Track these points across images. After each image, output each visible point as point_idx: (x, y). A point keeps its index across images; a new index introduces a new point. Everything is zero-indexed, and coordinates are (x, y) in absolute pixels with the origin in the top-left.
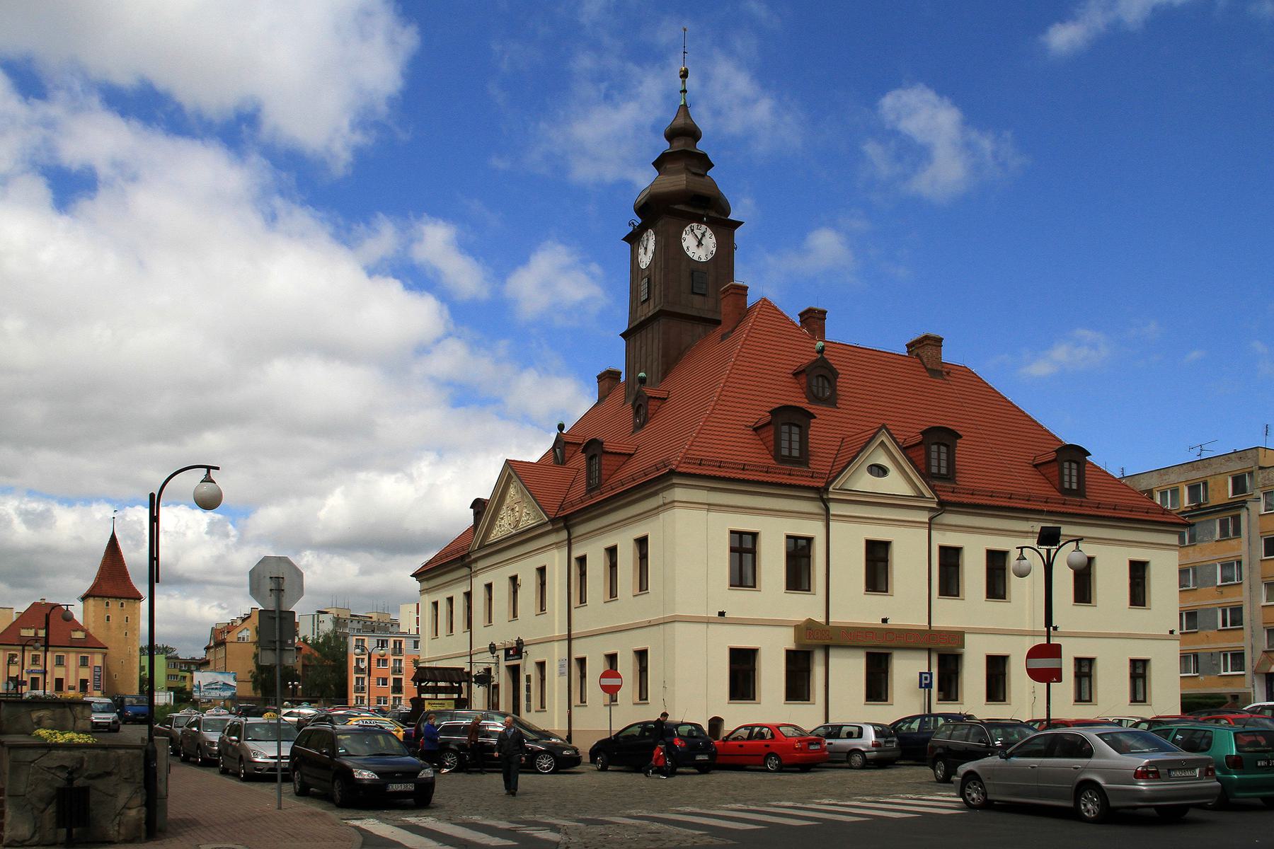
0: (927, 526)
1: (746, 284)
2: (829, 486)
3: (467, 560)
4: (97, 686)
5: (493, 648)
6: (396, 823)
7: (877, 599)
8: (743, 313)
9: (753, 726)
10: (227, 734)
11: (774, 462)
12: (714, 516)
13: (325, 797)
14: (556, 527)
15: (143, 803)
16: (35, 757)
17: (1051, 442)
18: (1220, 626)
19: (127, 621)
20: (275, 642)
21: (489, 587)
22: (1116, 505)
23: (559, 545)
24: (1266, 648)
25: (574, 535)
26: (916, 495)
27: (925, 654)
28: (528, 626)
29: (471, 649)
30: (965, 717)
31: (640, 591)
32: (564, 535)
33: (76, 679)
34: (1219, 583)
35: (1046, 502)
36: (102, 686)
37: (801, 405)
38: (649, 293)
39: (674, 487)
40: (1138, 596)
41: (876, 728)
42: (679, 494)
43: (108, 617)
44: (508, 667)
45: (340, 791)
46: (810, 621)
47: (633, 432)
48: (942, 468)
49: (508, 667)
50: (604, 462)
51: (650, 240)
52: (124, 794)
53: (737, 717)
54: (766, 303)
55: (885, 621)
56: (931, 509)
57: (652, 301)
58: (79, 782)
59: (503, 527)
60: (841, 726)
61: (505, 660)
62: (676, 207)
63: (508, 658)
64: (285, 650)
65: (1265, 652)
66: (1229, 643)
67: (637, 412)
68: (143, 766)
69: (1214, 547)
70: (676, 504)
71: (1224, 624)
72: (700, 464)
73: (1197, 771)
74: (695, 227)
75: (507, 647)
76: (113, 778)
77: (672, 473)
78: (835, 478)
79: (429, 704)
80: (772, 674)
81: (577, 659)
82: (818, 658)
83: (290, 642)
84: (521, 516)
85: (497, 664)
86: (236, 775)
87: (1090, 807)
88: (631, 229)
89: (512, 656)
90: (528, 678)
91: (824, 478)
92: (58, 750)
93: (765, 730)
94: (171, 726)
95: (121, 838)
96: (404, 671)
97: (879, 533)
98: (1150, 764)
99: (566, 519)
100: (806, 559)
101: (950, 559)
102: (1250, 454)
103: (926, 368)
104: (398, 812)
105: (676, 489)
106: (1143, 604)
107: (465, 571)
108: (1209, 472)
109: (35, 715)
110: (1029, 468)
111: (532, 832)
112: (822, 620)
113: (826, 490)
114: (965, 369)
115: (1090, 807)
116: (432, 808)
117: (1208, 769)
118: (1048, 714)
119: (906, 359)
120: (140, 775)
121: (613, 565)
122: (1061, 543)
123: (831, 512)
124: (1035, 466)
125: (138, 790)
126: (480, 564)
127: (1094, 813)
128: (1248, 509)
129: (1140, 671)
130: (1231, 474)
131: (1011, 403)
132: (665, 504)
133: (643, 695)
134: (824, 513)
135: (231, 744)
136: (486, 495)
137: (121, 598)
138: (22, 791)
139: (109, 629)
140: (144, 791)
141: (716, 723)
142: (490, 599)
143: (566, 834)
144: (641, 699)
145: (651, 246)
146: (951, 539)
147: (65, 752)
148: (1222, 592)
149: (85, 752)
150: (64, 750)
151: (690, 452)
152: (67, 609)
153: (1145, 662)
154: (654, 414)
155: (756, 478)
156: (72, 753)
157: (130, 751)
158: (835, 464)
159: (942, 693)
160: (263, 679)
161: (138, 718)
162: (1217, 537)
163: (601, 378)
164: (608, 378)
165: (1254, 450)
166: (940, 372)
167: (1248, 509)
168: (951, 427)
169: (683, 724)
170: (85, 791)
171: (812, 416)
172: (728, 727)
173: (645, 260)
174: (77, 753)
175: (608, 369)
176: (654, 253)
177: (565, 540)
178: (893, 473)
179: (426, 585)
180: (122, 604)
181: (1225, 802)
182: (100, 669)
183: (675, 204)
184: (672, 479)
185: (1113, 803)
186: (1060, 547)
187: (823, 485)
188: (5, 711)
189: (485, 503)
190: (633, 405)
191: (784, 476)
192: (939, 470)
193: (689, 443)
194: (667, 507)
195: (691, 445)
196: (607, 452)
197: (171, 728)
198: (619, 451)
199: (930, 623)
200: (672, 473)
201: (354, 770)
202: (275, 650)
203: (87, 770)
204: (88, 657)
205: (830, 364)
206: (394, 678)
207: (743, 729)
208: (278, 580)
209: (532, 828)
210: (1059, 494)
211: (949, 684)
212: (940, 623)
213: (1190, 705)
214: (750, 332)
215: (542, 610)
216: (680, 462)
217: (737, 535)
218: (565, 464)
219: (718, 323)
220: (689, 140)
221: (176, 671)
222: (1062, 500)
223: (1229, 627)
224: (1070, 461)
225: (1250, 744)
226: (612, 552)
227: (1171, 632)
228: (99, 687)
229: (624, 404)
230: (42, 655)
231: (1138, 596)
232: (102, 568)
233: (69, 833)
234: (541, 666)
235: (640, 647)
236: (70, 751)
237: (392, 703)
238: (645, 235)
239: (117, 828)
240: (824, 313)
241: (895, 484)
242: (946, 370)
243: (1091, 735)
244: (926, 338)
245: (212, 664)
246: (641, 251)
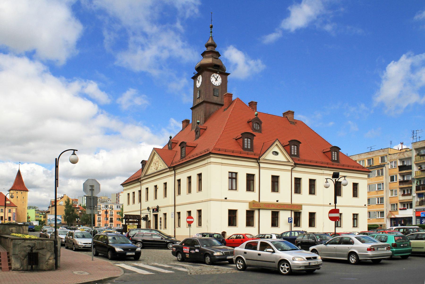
0: (291, 171)
2: (260, 158)
3: (140, 180)
4: (14, 219)
5: (148, 209)
6: (131, 265)
7: (275, 194)
8: (231, 102)
9: (237, 235)
10: (68, 236)
11: (242, 150)
12: (223, 167)
13: (105, 257)
14: (171, 170)
15: (54, 258)
16: (21, 242)
17: (329, 145)
18: (377, 203)
19: (23, 198)
20: (91, 207)
21: (147, 189)
22: (349, 166)
23: (171, 176)
24: (390, 210)
25: (176, 173)
26: (287, 161)
27: (290, 212)
28: (161, 202)
29: (141, 209)
30: (304, 232)
31: (199, 191)
32: (173, 172)
33: (7, 217)
34: (377, 190)
35: (327, 164)
36: (15, 219)
37: (250, 132)
39: (211, 158)
40: (355, 194)
41: (277, 235)
42: (212, 160)
43: (17, 197)
44: (154, 215)
45: (110, 255)
46: (254, 201)
47: (195, 140)
48: (293, 152)
49: (154, 215)
50: (186, 149)
51: (200, 78)
52: (48, 255)
53: (231, 232)
54: (238, 99)
55: (277, 201)
56: (292, 166)
57: (201, 98)
58: (34, 251)
59: (152, 170)
60: (265, 235)
61: (153, 212)
62: (209, 68)
63: (154, 212)
64: (94, 209)
65: (390, 211)
66: (380, 209)
67: (196, 132)
68: (54, 246)
69: (375, 179)
70: (211, 163)
71: (378, 203)
72: (219, 150)
73: (385, 248)
74: (215, 75)
75: (153, 208)
76: (45, 250)
77: (210, 153)
78: (262, 155)
79: (129, 226)
80: (241, 218)
81: (177, 213)
82: (256, 213)
83: (96, 206)
84: (158, 166)
85: (150, 214)
86: (72, 249)
87: (353, 260)
88: (194, 75)
89: (155, 211)
90: (161, 218)
91: (258, 155)
92: (27, 241)
93: (241, 236)
94: (46, 232)
95: (48, 269)
96: (113, 215)
97: (276, 173)
98: (372, 246)
99: (174, 167)
100: (277, 183)
101: (298, 181)
102: (386, 150)
103: (289, 121)
104: (130, 262)
106: (314, 194)
107: (139, 184)
108: (374, 155)
109: (11, 229)
110: (322, 153)
111: (177, 268)
112: (257, 200)
113: (259, 159)
114: (301, 122)
115: (353, 260)
116: (140, 260)
117: (388, 248)
118: (335, 231)
119: (282, 118)
120: (53, 249)
121: (190, 183)
122: (339, 178)
123: (261, 166)
124: (324, 153)
125: (53, 254)
126: (144, 181)
127: (354, 261)
128: (385, 167)
129: (355, 217)
130: (380, 156)
131: (315, 133)
132: (208, 163)
133: (200, 224)
134: (258, 166)
135: (70, 239)
136: (146, 159)
137: (21, 191)
138: (17, 253)
139: (17, 200)
140: (54, 254)
141: (224, 233)
142: (147, 193)
143: (188, 269)
144: (199, 225)
145: (201, 81)
146: (298, 176)
147: (30, 241)
148: (377, 193)
149: (36, 241)
150: (29, 241)
151: (216, 146)
152: (12, 194)
153: (314, 214)
155: (237, 155)
156: (32, 241)
157: (49, 241)
158: (262, 151)
159: (295, 224)
160: (67, 217)
161: (30, 230)
162: (376, 175)
164: (186, 122)
165: (387, 149)
166: (295, 122)
167: (385, 167)
168: (298, 140)
169: (215, 234)
170: (37, 254)
171: (254, 136)
172: (228, 235)
173: (198, 85)
174: (33, 242)
175: (185, 119)
176: (202, 83)
179: (125, 188)
180: (22, 193)
181: (392, 258)
182: (15, 214)
183: (208, 67)
184: (210, 155)
185: (360, 258)
186: (339, 179)
187: (258, 157)
188: (2, 227)
189: (145, 162)
190: (195, 131)
191: (238, 154)
192: (294, 153)
193: (215, 143)
194: (208, 164)
195: (216, 144)
196: (188, 146)
197: (46, 233)
198: (193, 146)
199: (291, 202)
201: (115, 248)
202: (91, 209)
203: (37, 247)
204: (11, 209)
205: (260, 119)
206: (110, 218)
207: (234, 236)
208: (92, 186)
209: (176, 267)
210: (331, 162)
211: (297, 221)
212: (295, 202)
213: (371, 228)
214: (234, 108)
215: (165, 197)
216: (213, 150)
217: (273, 177)
218: (172, 149)
219: (222, 105)
220: (213, 47)
221: (38, 215)
222: (332, 163)
223: (379, 204)
224: (335, 151)
225: (398, 240)
227: (365, 205)
228: (15, 219)
229: (191, 130)
230: (4, 209)
231: (355, 194)
233: (32, 267)
234: (165, 214)
235: (199, 209)
236: (31, 241)
237: (109, 226)
238: (198, 77)
239: (46, 266)
240: (256, 103)
241: (282, 157)
242: (295, 122)
243: (353, 237)
244: (289, 111)
245: (51, 212)
246: (197, 82)
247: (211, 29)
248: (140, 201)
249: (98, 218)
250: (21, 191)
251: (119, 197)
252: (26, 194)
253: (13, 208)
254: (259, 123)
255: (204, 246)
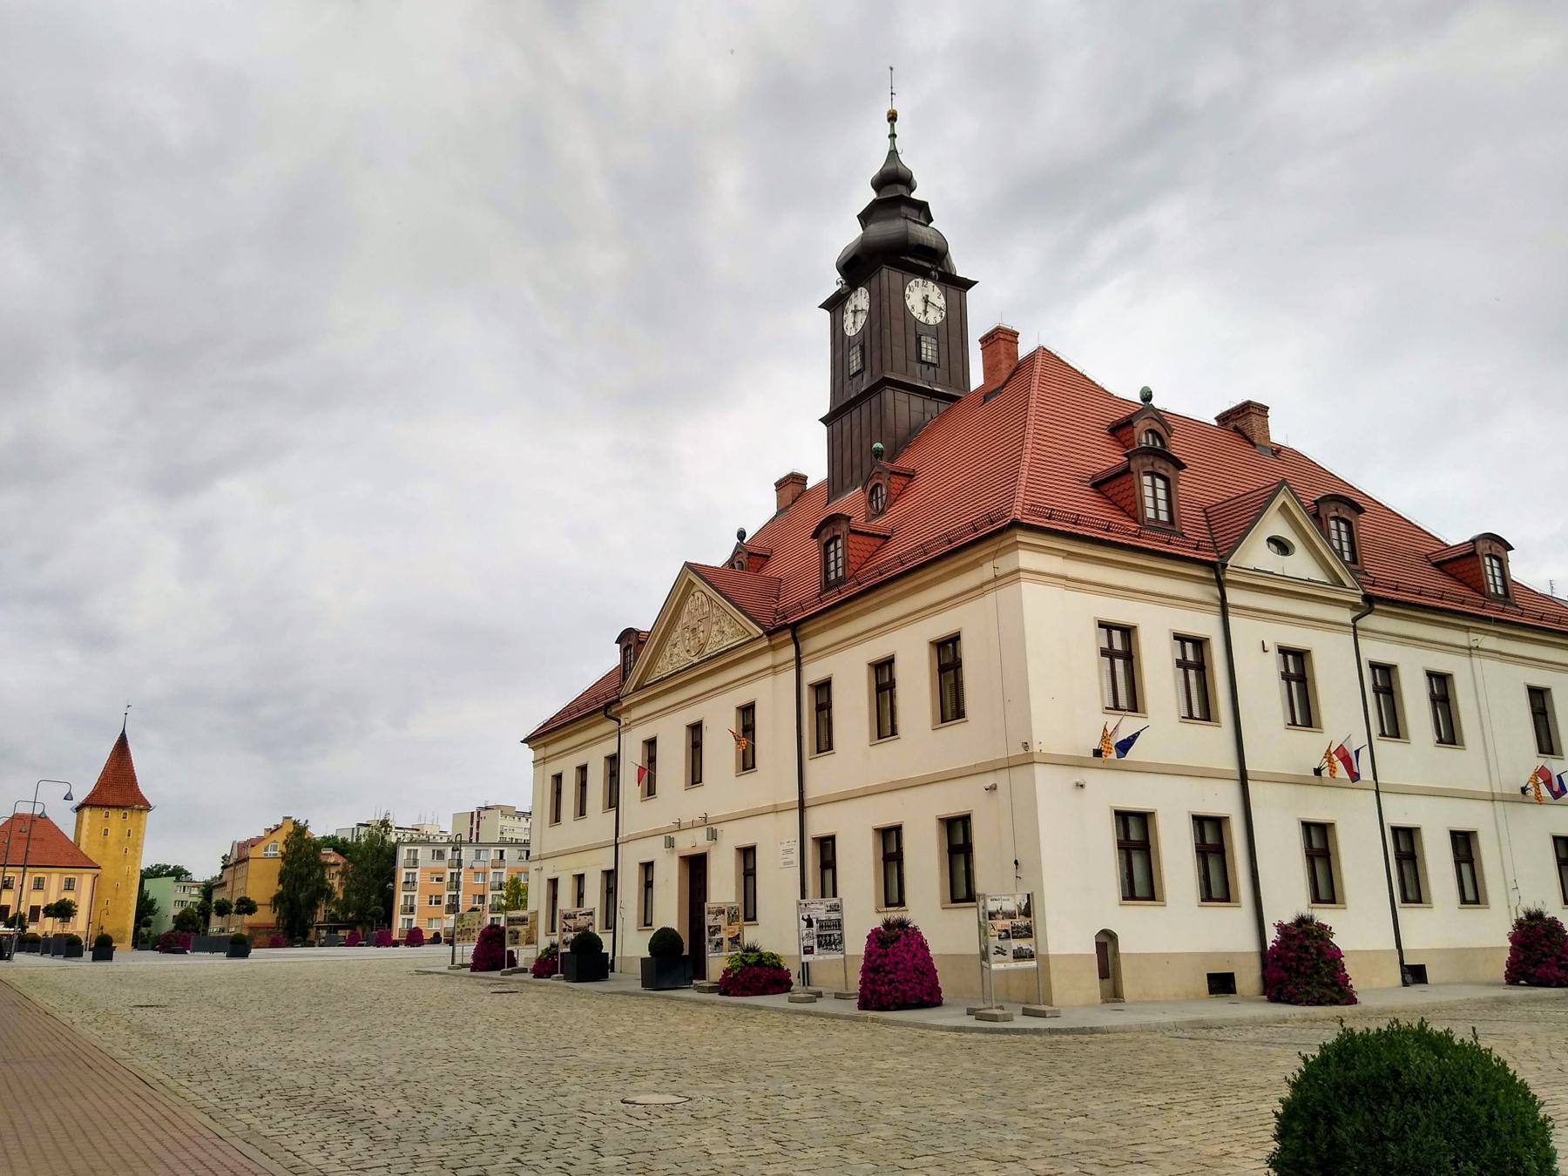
1: (1018, 331)
21: (651, 744)
38: (863, 359)
56: (1354, 606)
77: (1016, 525)
105: (1019, 551)
107: (611, 725)
126: (636, 713)
136: (645, 623)
139: (105, 844)
154: (898, 496)
163: (780, 485)
173: (853, 325)
177: (792, 660)
178: (1300, 551)
179: (542, 752)
200: (1016, 525)
226: (883, 671)
232: (105, 773)
241: (1300, 565)
247: (892, 126)
248: (613, 801)
249: (406, 897)
250: (120, 810)
251: (478, 822)
252: (141, 819)
253: (82, 874)
254: (1164, 434)
255: (1522, 982)
